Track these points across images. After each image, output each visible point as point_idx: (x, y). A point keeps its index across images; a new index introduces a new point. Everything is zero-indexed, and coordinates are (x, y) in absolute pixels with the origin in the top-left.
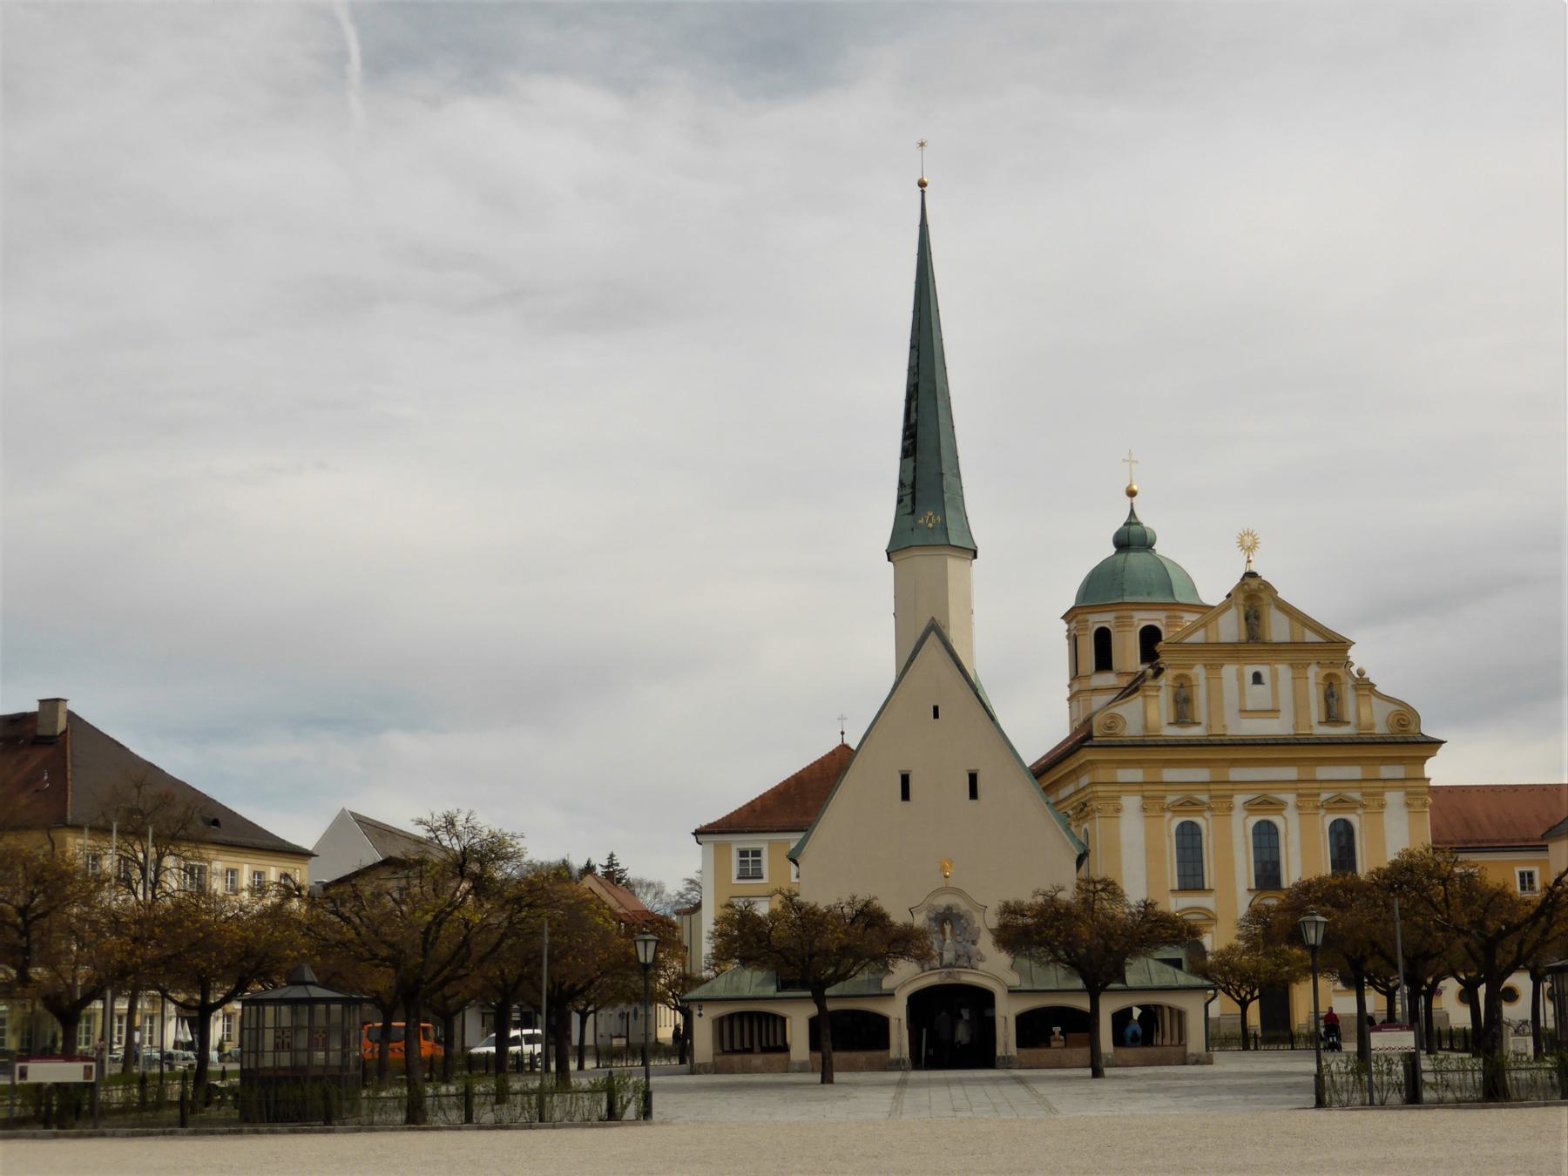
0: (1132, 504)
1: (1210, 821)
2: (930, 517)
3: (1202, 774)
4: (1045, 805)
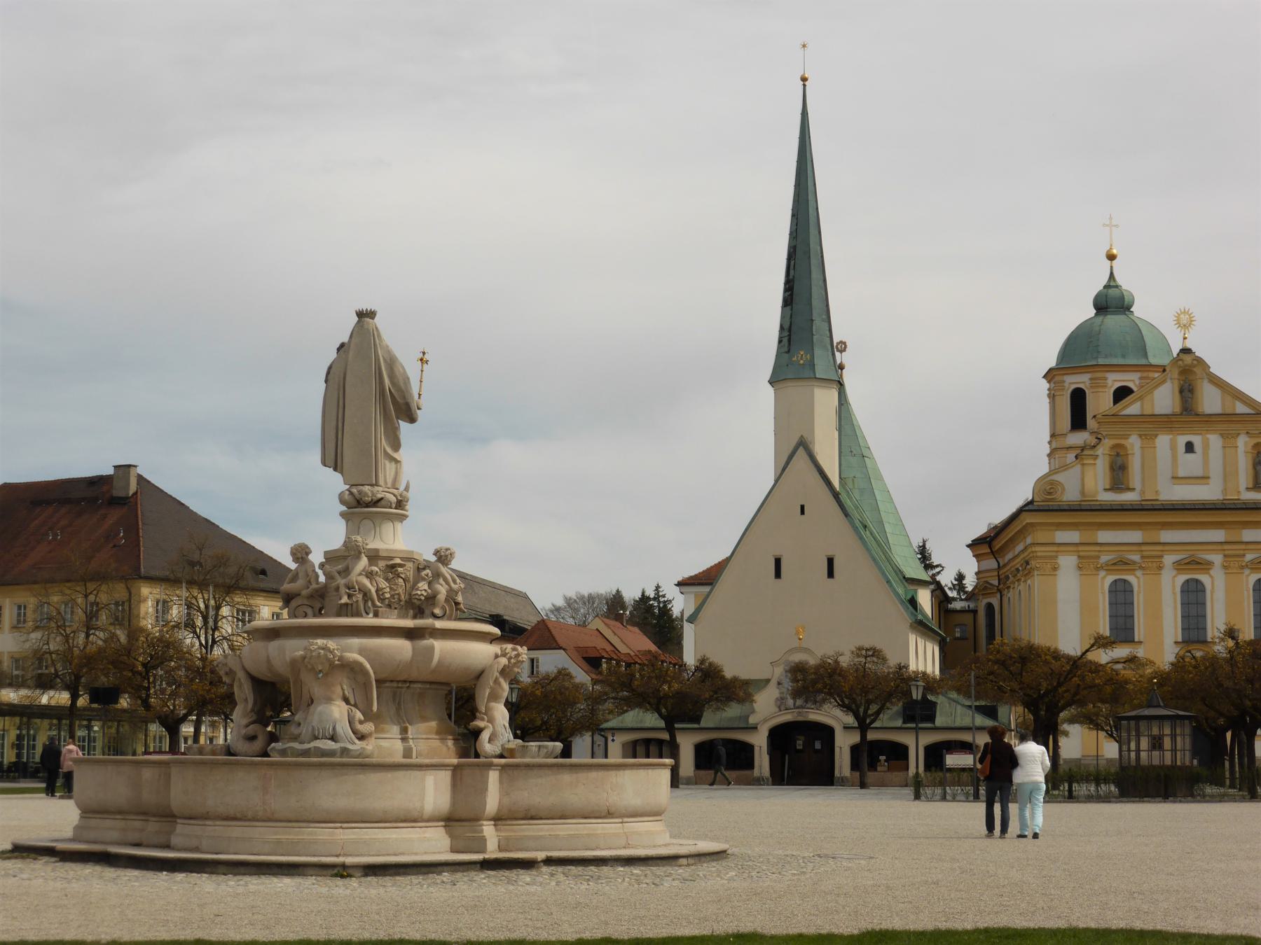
0: (1111, 267)
1: (1141, 580)
2: (802, 355)
3: (1135, 536)
4: (885, 583)
